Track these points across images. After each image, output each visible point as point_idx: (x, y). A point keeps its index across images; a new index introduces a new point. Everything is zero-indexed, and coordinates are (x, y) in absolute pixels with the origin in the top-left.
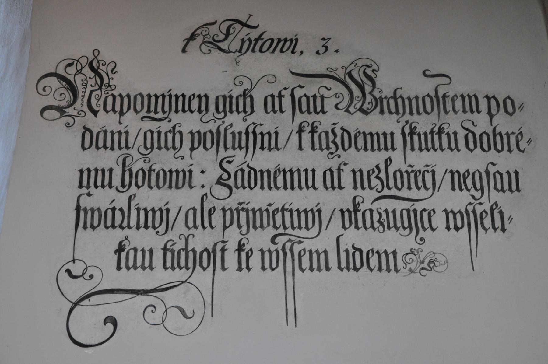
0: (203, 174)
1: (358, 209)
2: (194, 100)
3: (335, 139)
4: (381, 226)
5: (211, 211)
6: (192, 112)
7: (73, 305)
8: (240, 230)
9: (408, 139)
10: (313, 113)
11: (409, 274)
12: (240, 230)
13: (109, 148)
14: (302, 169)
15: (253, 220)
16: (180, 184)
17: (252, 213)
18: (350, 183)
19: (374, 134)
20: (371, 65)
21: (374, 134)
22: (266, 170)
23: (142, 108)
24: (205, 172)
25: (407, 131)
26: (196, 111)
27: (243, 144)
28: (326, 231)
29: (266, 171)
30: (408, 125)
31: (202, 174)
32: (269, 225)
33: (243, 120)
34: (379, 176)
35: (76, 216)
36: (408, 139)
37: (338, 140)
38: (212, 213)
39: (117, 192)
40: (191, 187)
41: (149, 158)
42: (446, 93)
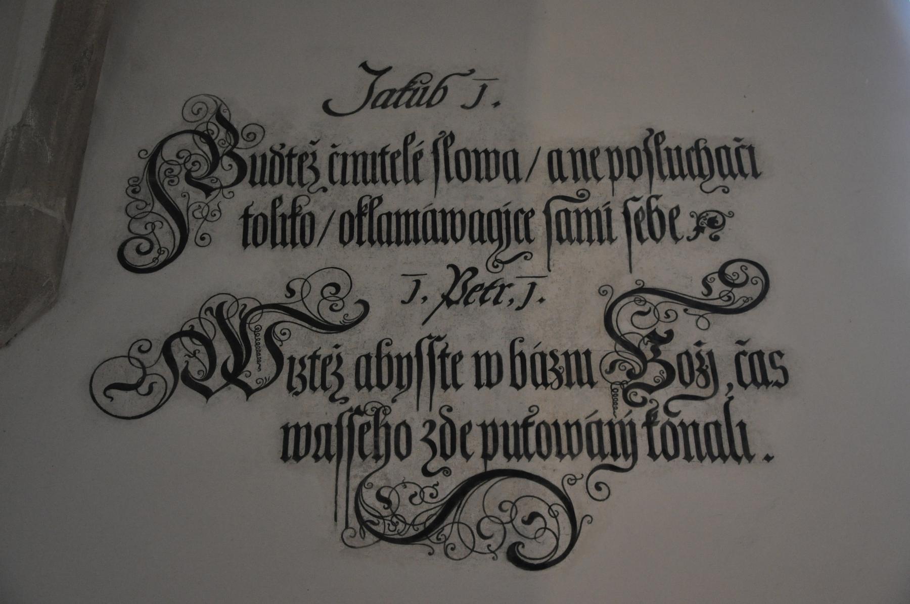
2: (330, 365)
3: (338, 368)
4: (701, 375)
5: (465, 428)
7: (431, 536)
9: (438, 362)
10: (300, 245)
11: (196, 128)
13: (668, 177)
17: (555, 174)
18: (754, 463)
27: (334, 449)
28: (597, 409)
30: (653, 136)
33: (693, 212)
35: (411, 444)
36: (438, 362)
37: (307, 373)
38: (467, 431)
39: (411, 426)
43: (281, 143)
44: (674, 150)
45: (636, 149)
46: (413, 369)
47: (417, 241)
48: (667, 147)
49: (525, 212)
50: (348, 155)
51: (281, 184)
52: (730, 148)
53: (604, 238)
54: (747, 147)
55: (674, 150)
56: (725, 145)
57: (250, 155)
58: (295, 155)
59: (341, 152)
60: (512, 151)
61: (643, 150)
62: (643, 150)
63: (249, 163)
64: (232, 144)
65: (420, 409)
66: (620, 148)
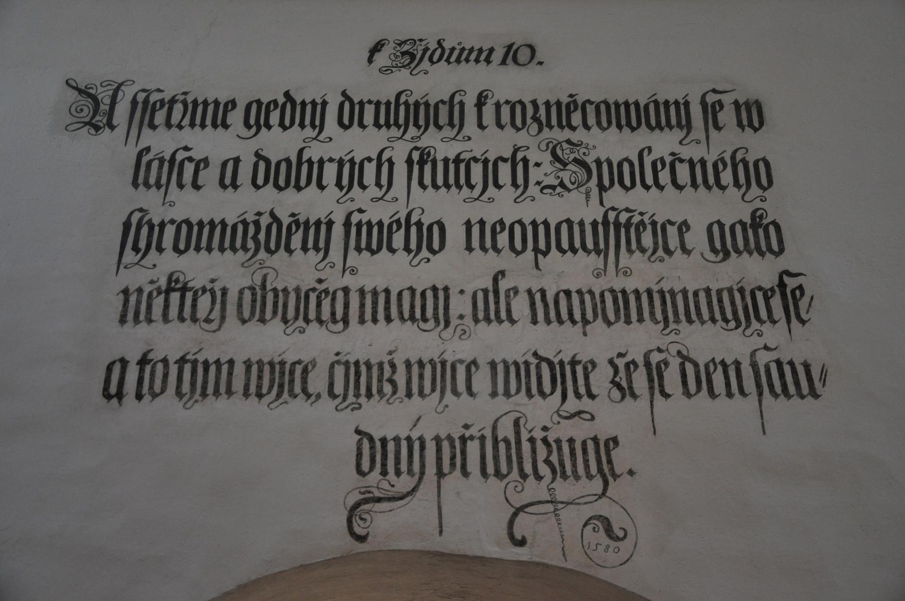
0: (507, 100)
1: (120, 91)
6: (723, 188)
8: (745, 155)
12: (745, 155)
14: (540, 102)
15: (760, 177)
16: (303, 182)
19: (631, 104)
20: (580, 143)
21: (631, 104)
22: (554, 102)
23: (748, 324)
24: (506, 64)
25: (416, 156)
26: (687, 186)
29: (555, 103)
31: (509, 100)
32: (423, 294)
34: (257, 159)
40: (321, 187)
41: (390, 58)
42: (459, 154)
43: (255, 213)
44: (404, 439)
45: (741, 222)
46: (294, 177)
47: (201, 224)
48: (536, 163)
49: (446, 102)
50: (494, 475)
51: (267, 187)
52: (415, 290)
53: (317, 164)
54: (477, 437)
55: (404, 439)
56: (360, 208)
57: (471, 476)
58: (579, 362)
59: (344, 360)
60: (408, 289)
61: (612, 223)
62: (612, 223)
63: (594, 167)
64: (404, 64)
65: (351, 150)
66: (599, 437)
